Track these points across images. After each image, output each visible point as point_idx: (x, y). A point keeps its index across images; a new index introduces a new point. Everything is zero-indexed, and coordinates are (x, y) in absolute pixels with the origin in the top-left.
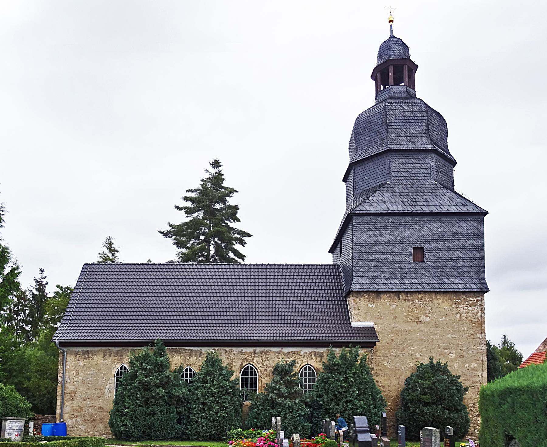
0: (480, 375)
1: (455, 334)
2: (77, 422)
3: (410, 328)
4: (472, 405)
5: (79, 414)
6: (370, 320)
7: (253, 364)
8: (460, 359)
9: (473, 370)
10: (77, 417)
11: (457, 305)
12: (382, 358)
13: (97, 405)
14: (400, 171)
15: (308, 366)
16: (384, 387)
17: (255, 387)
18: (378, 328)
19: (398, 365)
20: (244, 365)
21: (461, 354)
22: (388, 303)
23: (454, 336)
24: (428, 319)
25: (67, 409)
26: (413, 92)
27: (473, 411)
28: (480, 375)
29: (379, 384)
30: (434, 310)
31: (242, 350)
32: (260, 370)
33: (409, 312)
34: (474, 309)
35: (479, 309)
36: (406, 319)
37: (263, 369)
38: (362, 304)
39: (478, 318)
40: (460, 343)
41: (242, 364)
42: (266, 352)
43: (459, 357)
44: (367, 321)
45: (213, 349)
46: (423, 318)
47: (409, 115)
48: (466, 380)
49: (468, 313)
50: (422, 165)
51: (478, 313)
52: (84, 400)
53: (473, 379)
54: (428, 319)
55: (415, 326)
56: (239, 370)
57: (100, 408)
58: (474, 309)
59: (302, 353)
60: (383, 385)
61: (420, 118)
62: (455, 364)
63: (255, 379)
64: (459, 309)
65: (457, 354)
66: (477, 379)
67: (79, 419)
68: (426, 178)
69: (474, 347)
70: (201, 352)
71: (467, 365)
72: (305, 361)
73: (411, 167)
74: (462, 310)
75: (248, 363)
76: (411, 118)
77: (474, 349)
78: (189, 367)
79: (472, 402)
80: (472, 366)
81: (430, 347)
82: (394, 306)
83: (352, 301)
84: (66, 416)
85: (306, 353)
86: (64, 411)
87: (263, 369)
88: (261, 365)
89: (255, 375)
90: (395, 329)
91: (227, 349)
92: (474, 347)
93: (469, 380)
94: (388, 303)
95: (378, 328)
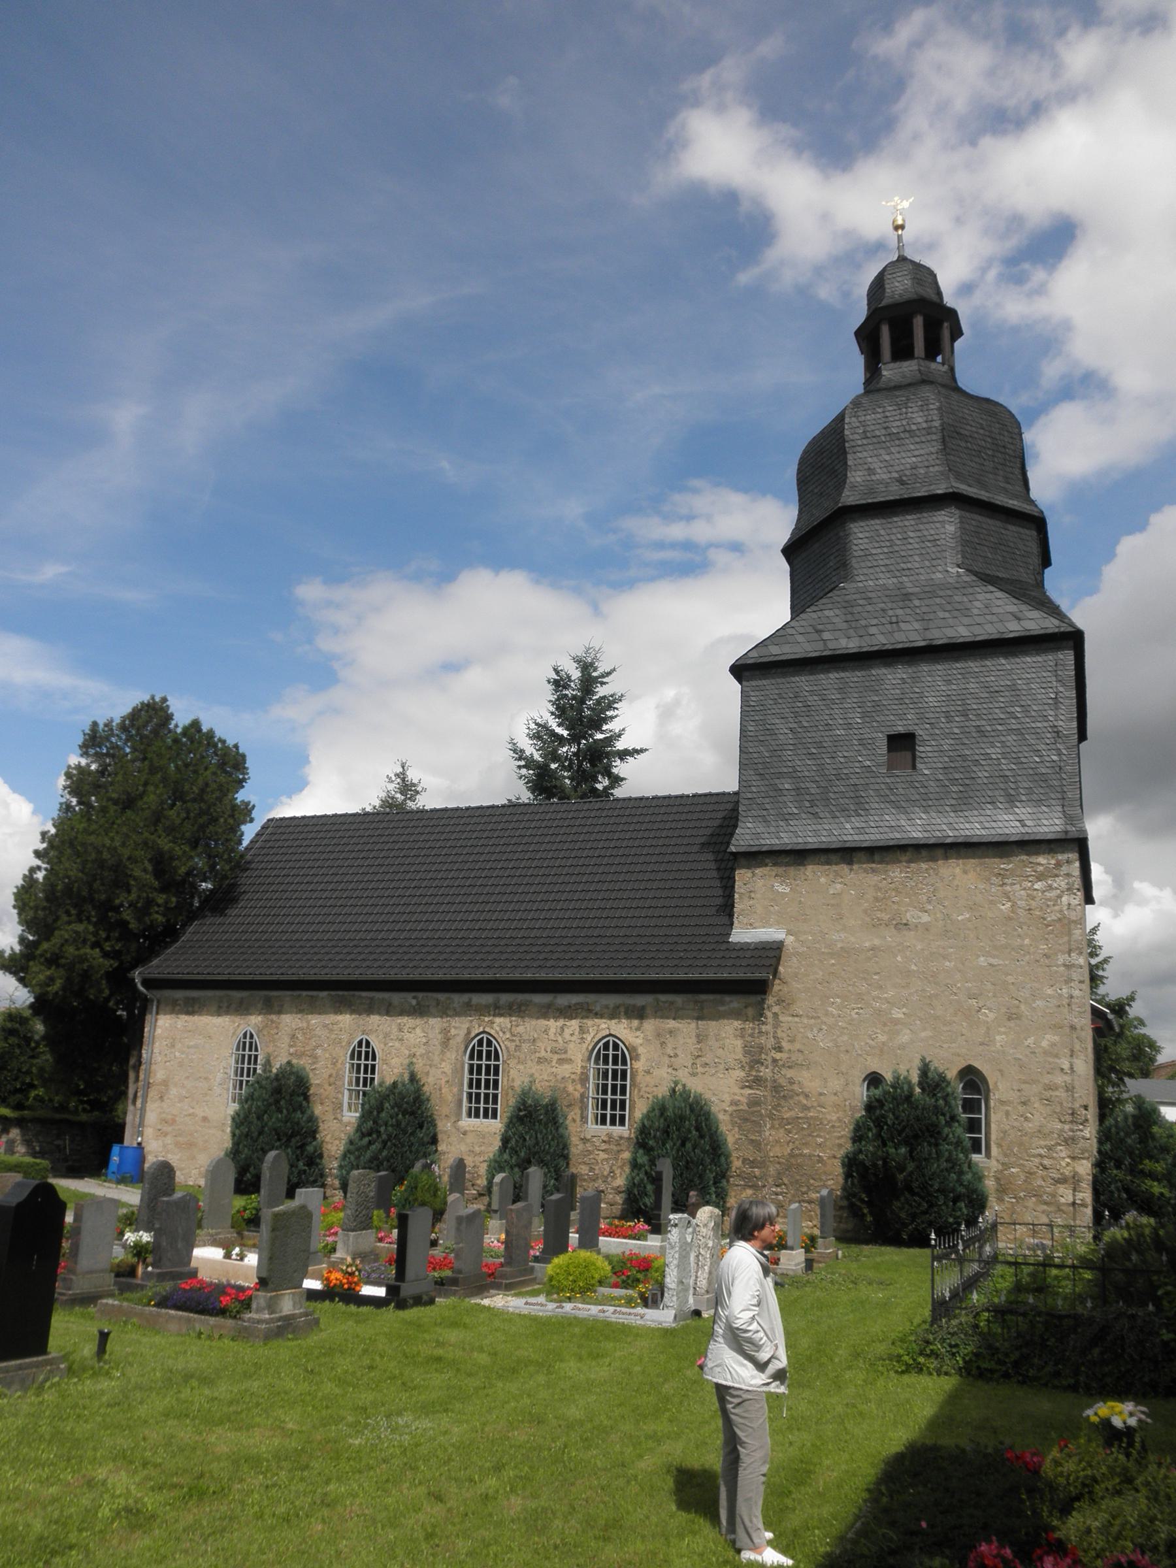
0: (1066, 1066)
1: (994, 957)
2: (164, 1146)
3: (877, 942)
4: (1042, 1151)
5: (170, 1129)
6: (778, 923)
7: (493, 1032)
8: (1012, 1024)
9: (1045, 1053)
10: (166, 1134)
11: (1003, 876)
12: (805, 1021)
13: (200, 1112)
14: (871, 555)
15: (611, 1039)
16: (807, 1096)
17: (496, 1087)
18: (796, 945)
19: (845, 1038)
20: (473, 1035)
21: (1014, 1011)
22: (823, 880)
23: (994, 961)
24: (925, 918)
25: (151, 1117)
26: (169, 1304)
27: (1045, 1168)
28: (1066, 1066)
29: (796, 1087)
30: (941, 894)
31: (470, 1000)
32: (507, 1048)
33: (877, 899)
34: (1050, 887)
35: (1063, 884)
36: (868, 919)
37: (512, 1046)
38: (760, 883)
39: (1061, 911)
40: (1010, 979)
41: (469, 1033)
42: (520, 1006)
43: (1009, 1019)
44: (771, 926)
45: (414, 998)
46: (911, 915)
47: (898, 423)
48: (1025, 1082)
49: (1033, 898)
50: (926, 533)
51: (1060, 897)
52: (180, 1101)
53: (1046, 1079)
54: (925, 918)
55: (890, 937)
56: (463, 1047)
57: (205, 1119)
58: (1050, 887)
59: (598, 1009)
60: (807, 1090)
61: (925, 425)
62: (998, 1038)
63: (497, 1068)
64: (1008, 888)
65: (1004, 1010)
66: (1059, 1079)
67: (169, 1140)
68: (934, 563)
69: (1049, 991)
70: (390, 1005)
71: (1030, 1041)
72: (603, 1026)
73: (898, 542)
74: (1018, 891)
75: (481, 1029)
76: (902, 429)
77: (1050, 996)
78: (365, 1037)
79: (1042, 1143)
80: (1045, 1044)
81: (930, 990)
82: (839, 886)
83: (742, 877)
84: (149, 1132)
85: (607, 1007)
86: (147, 1122)
87: (512, 1046)
88: (508, 1036)
89: (497, 1058)
90: (839, 945)
91: (442, 997)
92: (1049, 991)
93: (1035, 1082)
94: (823, 880)
95: (796, 945)
